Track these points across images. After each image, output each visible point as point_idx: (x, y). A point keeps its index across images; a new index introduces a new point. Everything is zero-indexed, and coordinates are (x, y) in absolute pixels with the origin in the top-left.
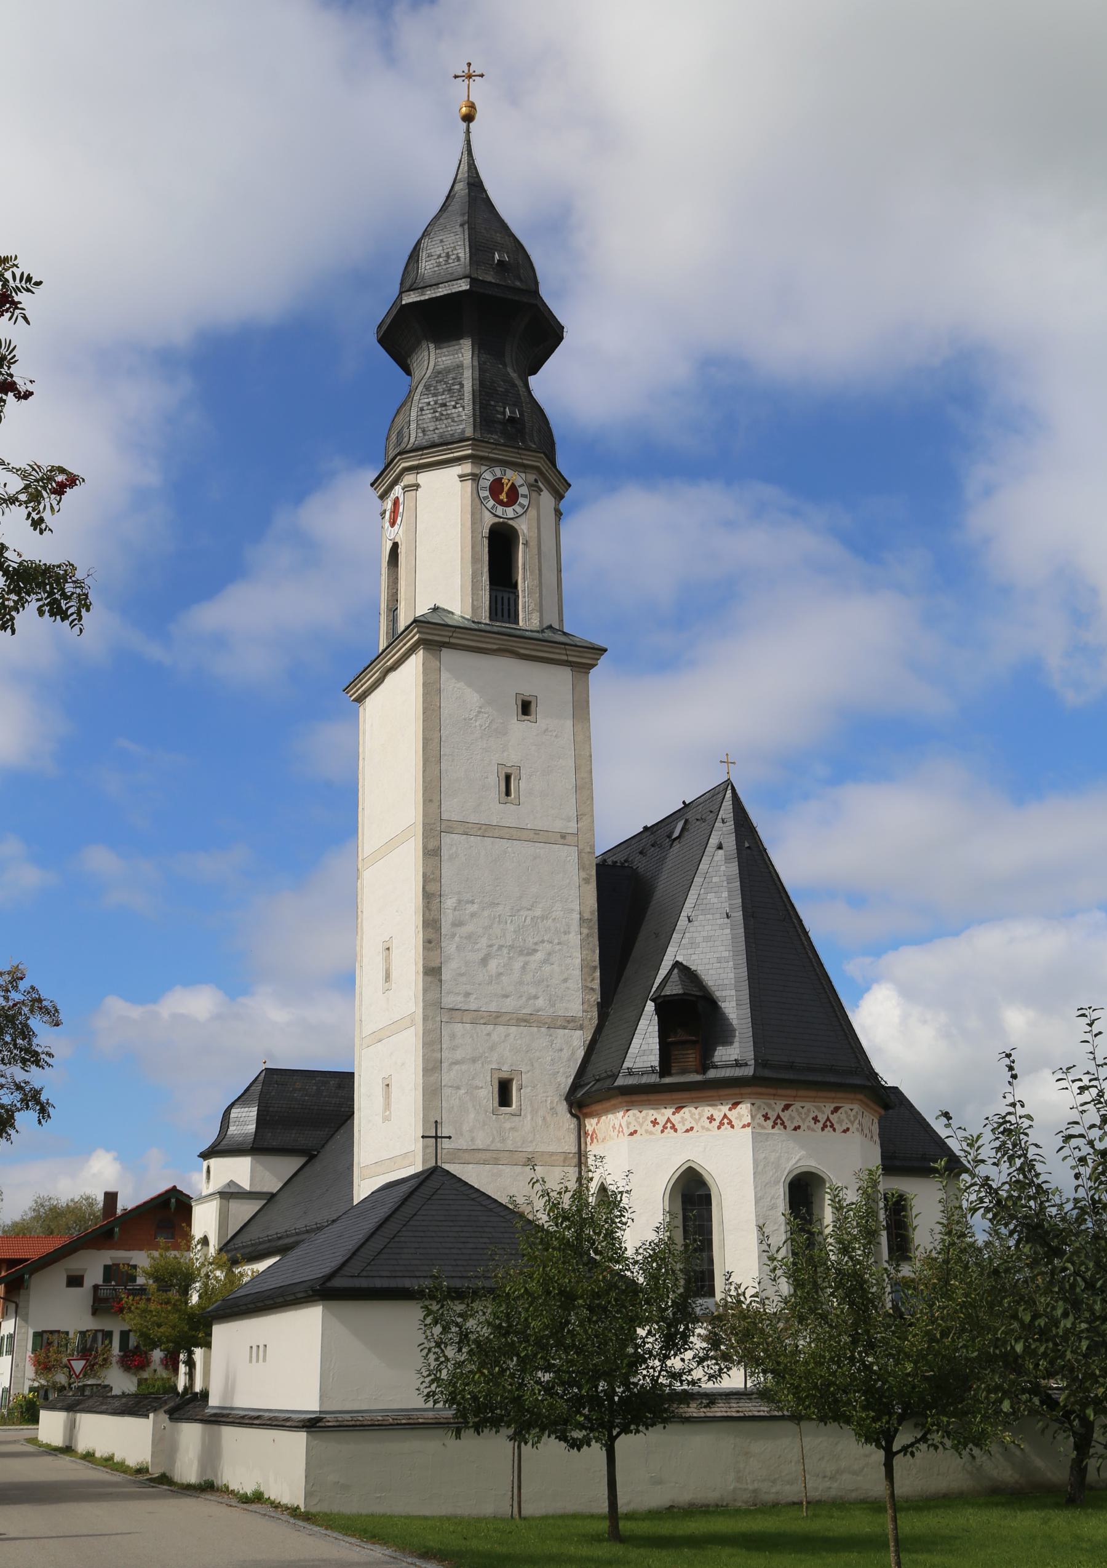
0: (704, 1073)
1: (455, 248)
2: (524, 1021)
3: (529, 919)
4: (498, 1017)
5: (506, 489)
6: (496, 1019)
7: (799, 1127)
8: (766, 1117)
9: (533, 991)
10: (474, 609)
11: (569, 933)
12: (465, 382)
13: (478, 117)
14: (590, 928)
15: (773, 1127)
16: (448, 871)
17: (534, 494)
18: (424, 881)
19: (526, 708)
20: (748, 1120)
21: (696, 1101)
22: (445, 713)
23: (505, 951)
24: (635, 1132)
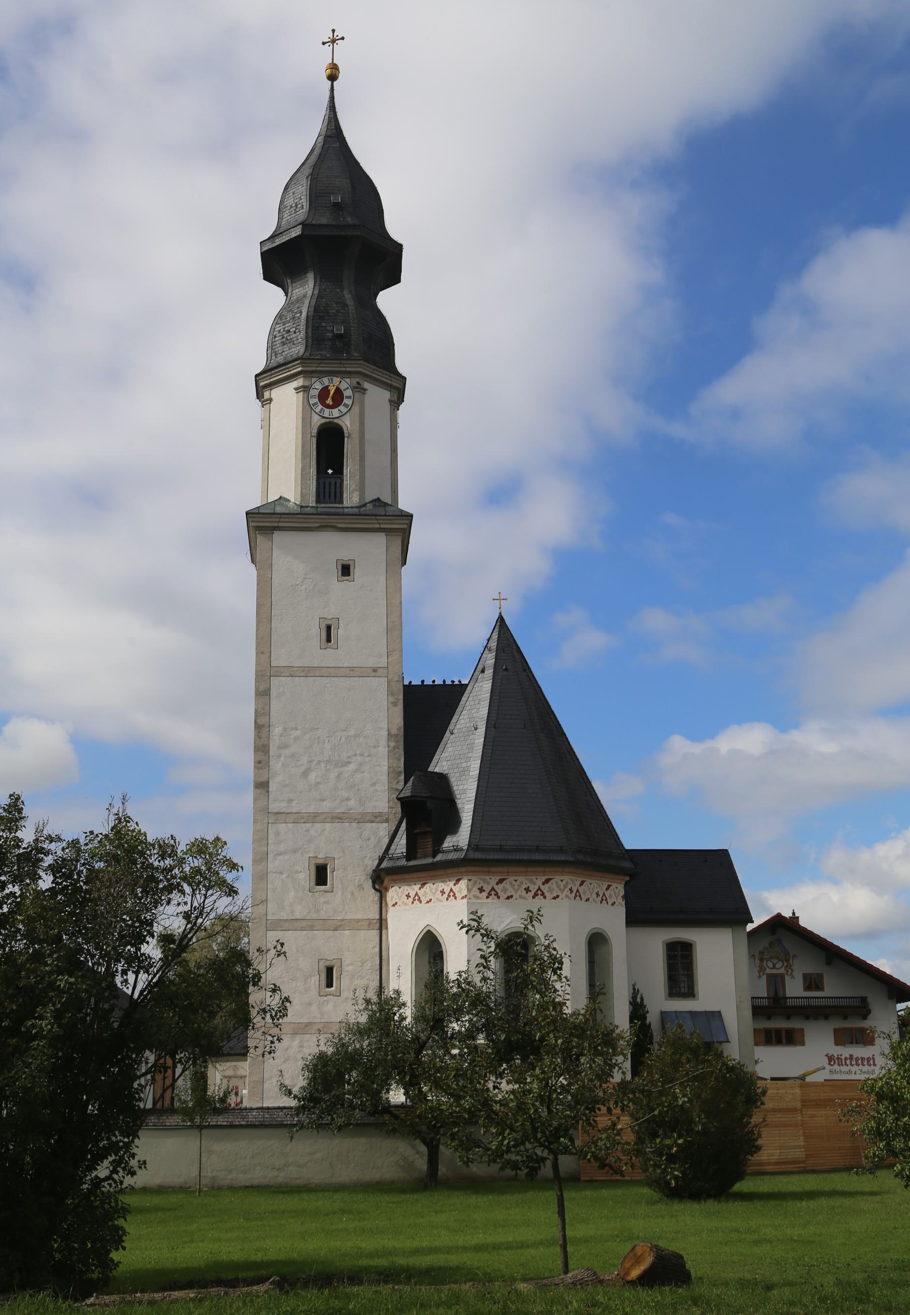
0: (434, 857)
1: (301, 199)
2: (338, 818)
3: (343, 740)
4: (315, 817)
5: (332, 393)
6: (314, 818)
7: (512, 896)
8: (481, 890)
9: (345, 794)
10: (303, 496)
11: (378, 746)
13: (341, 76)
14: (397, 741)
15: (487, 897)
16: (275, 706)
17: (357, 395)
18: (256, 716)
19: (346, 570)
20: (465, 892)
21: (434, 879)
22: (275, 582)
23: (323, 765)
24: (396, 903)
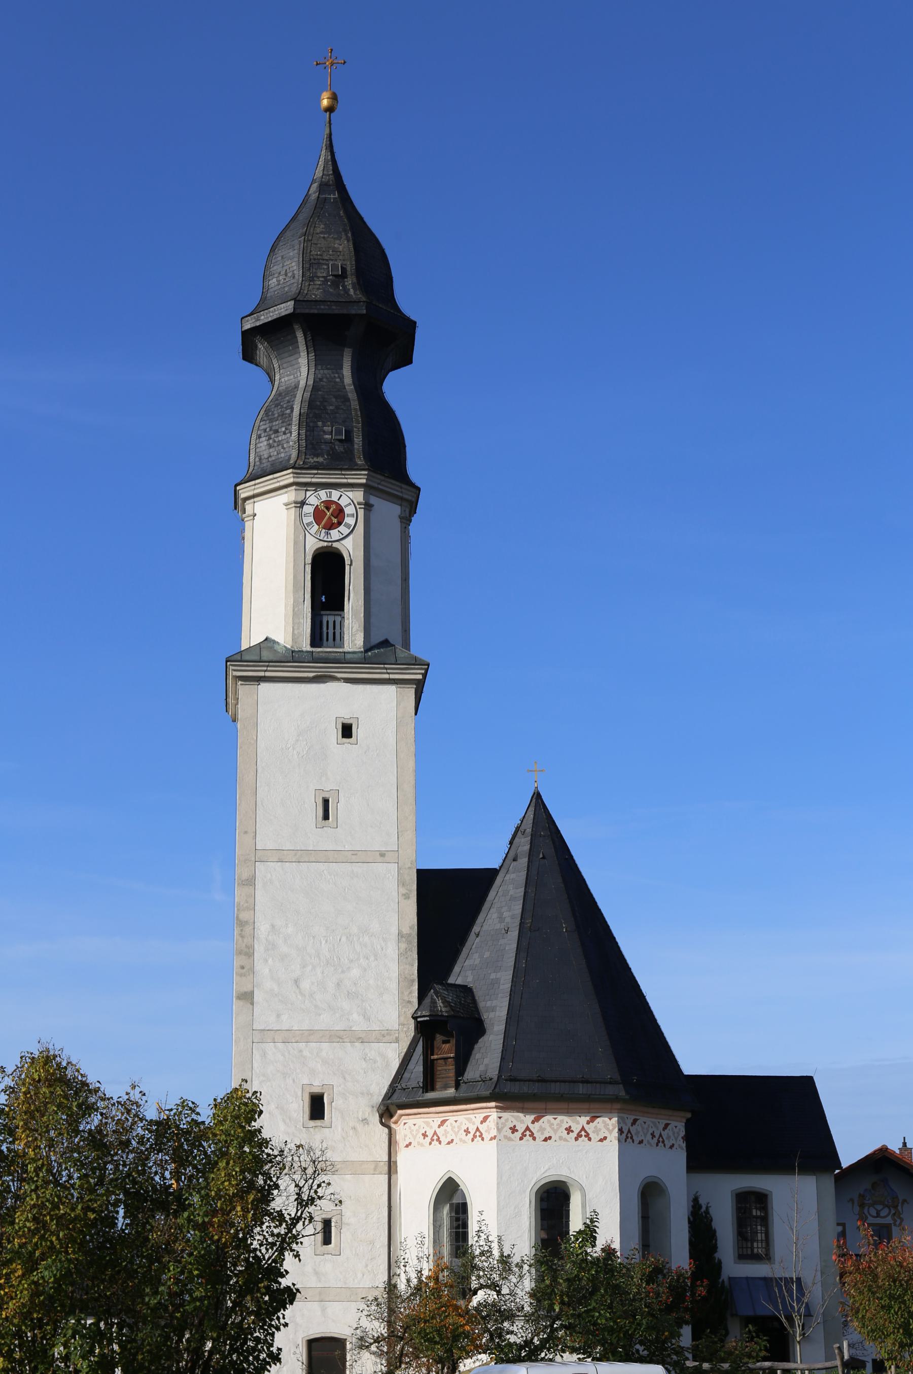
2: (336, 1037)
6: (308, 1036)
7: (550, 1138)
10: (294, 639)
12: (295, 407)
20: (494, 1132)
22: (261, 744)
